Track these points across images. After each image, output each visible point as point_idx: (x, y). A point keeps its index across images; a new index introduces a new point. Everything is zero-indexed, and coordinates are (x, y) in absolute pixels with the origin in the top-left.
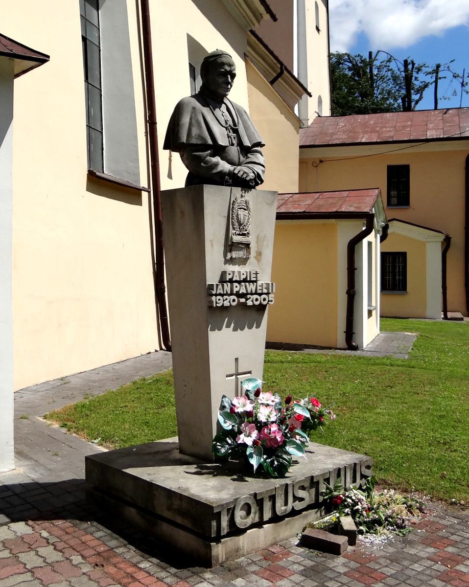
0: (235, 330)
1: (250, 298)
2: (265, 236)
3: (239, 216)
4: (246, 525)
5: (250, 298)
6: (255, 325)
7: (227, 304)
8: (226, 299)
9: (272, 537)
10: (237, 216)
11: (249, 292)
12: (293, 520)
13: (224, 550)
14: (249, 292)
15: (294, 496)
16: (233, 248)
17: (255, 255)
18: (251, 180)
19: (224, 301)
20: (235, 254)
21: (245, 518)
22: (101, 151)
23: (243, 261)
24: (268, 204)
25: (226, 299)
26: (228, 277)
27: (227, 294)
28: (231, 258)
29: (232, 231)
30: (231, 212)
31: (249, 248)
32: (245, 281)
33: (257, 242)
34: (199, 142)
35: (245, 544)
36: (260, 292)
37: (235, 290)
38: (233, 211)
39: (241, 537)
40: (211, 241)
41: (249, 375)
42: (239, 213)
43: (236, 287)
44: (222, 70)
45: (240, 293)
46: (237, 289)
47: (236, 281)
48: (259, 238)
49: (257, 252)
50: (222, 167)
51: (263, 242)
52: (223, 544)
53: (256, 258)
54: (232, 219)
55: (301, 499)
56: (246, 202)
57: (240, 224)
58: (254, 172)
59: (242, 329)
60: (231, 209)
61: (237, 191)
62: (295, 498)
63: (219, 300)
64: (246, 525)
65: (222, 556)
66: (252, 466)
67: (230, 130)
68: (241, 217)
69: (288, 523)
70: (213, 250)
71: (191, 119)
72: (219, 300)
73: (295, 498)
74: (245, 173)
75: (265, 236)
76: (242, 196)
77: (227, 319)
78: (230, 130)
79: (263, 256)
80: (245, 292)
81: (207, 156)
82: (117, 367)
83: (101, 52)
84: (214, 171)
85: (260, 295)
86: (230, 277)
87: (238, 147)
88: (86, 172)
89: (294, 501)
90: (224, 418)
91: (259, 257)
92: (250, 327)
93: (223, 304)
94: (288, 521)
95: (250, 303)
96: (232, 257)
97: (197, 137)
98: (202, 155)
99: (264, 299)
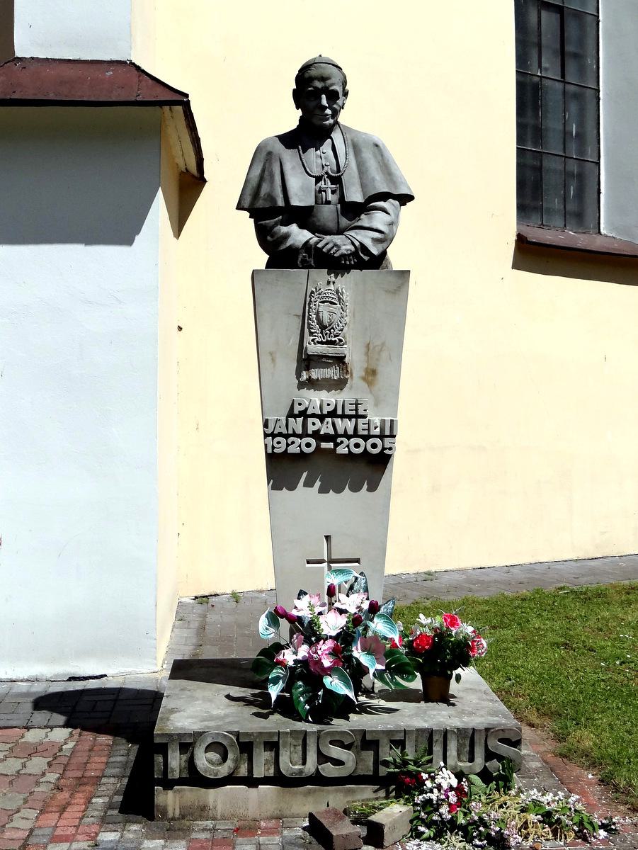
0: (323, 490)
1: (342, 442)
2: (383, 344)
3: (321, 315)
4: (216, 774)
5: (342, 442)
6: (365, 486)
7: (293, 449)
8: (293, 443)
9: (274, 806)
10: (317, 314)
11: (341, 431)
12: (323, 791)
13: (178, 802)
14: (341, 431)
15: (319, 753)
16: (312, 363)
18: (343, 256)
19: (288, 445)
20: (315, 373)
21: (220, 764)
22: (596, 196)
23: (339, 384)
24: (387, 291)
25: (293, 443)
26: (297, 409)
27: (294, 435)
28: (309, 379)
29: (308, 338)
30: (307, 308)
31: (344, 363)
32: (333, 414)
33: (367, 354)
34: (267, 205)
35: (219, 802)
36: (366, 433)
37: (311, 429)
38: (310, 307)
39: (212, 791)
40: (271, 354)
41: (357, 564)
42: (320, 310)
43: (314, 424)
44: (310, 89)
45: (322, 433)
46: (315, 428)
47: (313, 415)
49: (367, 369)
50: (293, 239)
52: (175, 792)
53: (364, 379)
54: (309, 319)
55: (338, 762)
56: (337, 292)
57: (323, 327)
58: (353, 244)
59: (339, 490)
60: (307, 304)
61: (320, 277)
62: (323, 758)
63: (279, 443)
64: (216, 774)
67: (327, 179)
68: (326, 319)
69: (309, 792)
70: (274, 366)
71: (263, 170)
72: (279, 443)
73: (323, 758)
74: (335, 245)
75: (383, 344)
76: (329, 283)
77: (305, 474)
78: (327, 179)
79: (379, 377)
80: (332, 432)
81: (276, 224)
82: (538, 567)
83: (600, 23)
84: (283, 247)
85: (366, 438)
86: (302, 408)
87: (339, 206)
88: (514, 238)
89: (320, 762)
90: (269, 622)
91: (370, 378)
92: (356, 488)
93: (286, 449)
95: (342, 450)
96: (310, 377)
97: (266, 196)
98: (268, 223)
99: (374, 446)
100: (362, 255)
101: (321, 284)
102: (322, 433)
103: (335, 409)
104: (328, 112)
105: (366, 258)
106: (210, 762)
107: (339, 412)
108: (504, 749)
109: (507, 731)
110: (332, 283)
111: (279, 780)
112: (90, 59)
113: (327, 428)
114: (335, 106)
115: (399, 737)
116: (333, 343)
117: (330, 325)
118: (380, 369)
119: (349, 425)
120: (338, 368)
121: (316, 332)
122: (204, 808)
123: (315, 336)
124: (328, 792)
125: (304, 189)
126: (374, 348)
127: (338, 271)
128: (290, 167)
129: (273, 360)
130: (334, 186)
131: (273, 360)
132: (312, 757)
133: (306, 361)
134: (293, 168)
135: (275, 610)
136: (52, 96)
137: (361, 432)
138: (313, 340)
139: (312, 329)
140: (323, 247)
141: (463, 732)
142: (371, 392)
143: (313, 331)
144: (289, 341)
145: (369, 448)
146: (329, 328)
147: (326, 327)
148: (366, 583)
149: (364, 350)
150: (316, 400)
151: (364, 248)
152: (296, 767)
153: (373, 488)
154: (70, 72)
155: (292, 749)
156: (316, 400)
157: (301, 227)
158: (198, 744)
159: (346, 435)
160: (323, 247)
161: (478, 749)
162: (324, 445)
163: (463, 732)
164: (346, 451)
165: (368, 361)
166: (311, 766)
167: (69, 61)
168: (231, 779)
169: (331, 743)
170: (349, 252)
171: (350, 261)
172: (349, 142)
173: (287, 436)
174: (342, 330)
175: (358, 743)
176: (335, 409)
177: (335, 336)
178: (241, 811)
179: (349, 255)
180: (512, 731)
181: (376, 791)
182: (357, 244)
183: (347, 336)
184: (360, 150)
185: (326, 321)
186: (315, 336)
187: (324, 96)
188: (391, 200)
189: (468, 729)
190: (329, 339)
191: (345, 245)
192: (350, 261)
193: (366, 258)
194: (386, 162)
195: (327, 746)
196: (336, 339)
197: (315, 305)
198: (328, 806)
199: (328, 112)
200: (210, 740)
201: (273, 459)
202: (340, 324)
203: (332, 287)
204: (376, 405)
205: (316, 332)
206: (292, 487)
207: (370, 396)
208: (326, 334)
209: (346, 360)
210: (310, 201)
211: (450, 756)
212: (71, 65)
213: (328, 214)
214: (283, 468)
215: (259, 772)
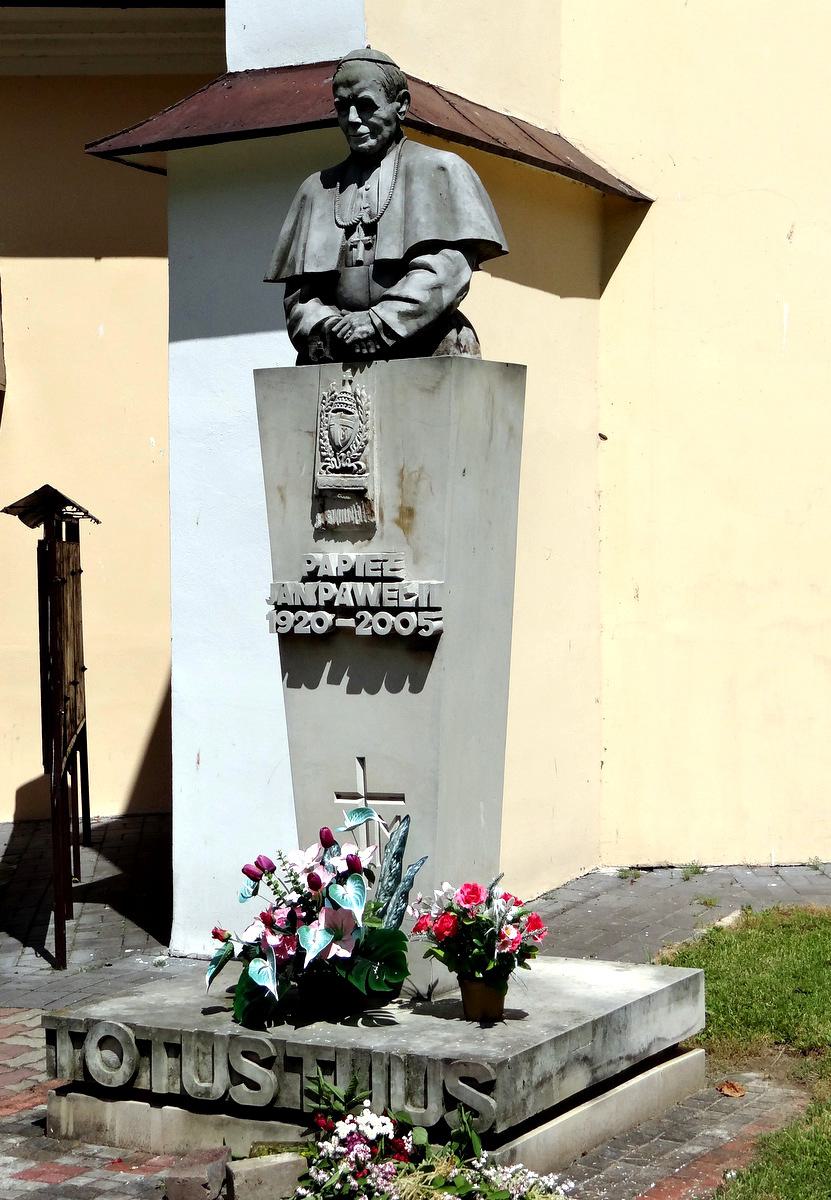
0: (352, 690)
2: (422, 469)
5: (362, 618)
6: (407, 685)
12: (238, 1124)
17: (396, 515)
18: (357, 341)
20: (335, 516)
24: (424, 390)
28: (325, 525)
31: (366, 500)
32: (350, 576)
33: (400, 485)
36: (394, 604)
37: (324, 597)
39: (109, 1105)
45: (336, 604)
46: (329, 597)
48: (406, 474)
49: (401, 508)
51: (416, 483)
53: (398, 523)
55: (253, 1085)
57: (336, 449)
59: (373, 690)
62: (236, 1078)
64: (110, 1082)
65: (68, 1124)
66: (264, 989)
70: (285, 507)
73: (236, 1078)
75: (422, 469)
77: (328, 665)
79: (419, 519)
91: (407, 521)
92: (395, 688)
93: (292, 629)
94: (223, 1120)
95: (363, 630)
96: (326, 522)
100: (385, 338)
101: (335, 384)
102: (336, 604)
103: (353, 570)
104: (364, 129)
105: (390, 342)
106: (106, 1063)
107: (359, 573)
108: (468, 1094)
109: (471, 1067)
110: (347, 383)
111: (182, 1100)
112: (315, 61)
113: (344, 595)
114: (372, 120)
115: (328, 1057)
116: (349, 470)
117: (345, 444)
118: (418, 508)
119: (367, 592)
120: (359, 507)
121: (328, 456)
122: (100, 1128)
123: (327, 461)
124: (245, 1127)
125: (326, 247)
126: (410, 475)
127: (356, 364)
128: (319, 215)
129: (283, 498)
130: (368, 238)
131: (283, 498)
132: (222, 1076)
133: (323, 499)
134: (322, 217)
135: (256, 863)
136: (226, 129)
137: (387, 603)
138: (324, 468)
139: (324, 451)
140: (339, 330)
141: (415, 1061)
142: (408, 543)
143: (324, 454)
144: (301, 468)
145: (400, 628)
146: (344, 449)
147: (339, 448)
148: (407, 830)
149: (397, 479)
150: (335, 556)
151: (386, 328)
152: (203, 1085)
153: (416, 688)
154: (278, 84)
155: (201, 1058)
156: (335, 556)
157: (326, 302)
158: (89, 1036)
159: (367, 608)
160: (339, 330)
161: (432, 1088)
162: (341, 622)
163: (415, 1061)
164: (368, 631)
165: (402, 497)
166: (218, 1085)
167: (291, 68)
168: (127, 1091)
169: (246, 1054)
170: (365, 336)
171: (368, 348)
172: (402, 168)
173: (294, 609)
174: (361, 451)
175: (280, 1060)
176: (353, 570)
177: (353, 461)
178: (143, 1138)
179: (365, 340)
180: (479, 1068)
181: (303, 1135)
182: (377, 322)
183: (369, 460)
184: (411, 180)
185: (339, 441)
186: (327, 461)
187: (353, 108)
188: (447, 251)
189: (422, 1056)
190: (344, 465)
191: (361, 325)
192: (368, 348)
193: (390, 342)
194: (452, 191)
195: (238, 1058)
196: (353, 464)
197: (327, 416)
198: (224, 1144)
199: (364, 129)
200: (101, 1033)
201: (289, 642)
202: (358, 443)
203: (348, 388)
204: (416, 561)
205: (328, 456)
206: (313, 684)
207: (407, 548)
208: (341, 458)
209: (369, 495)
210: (330, 264)
211: (395, 1094)
212: (289, 75)
213: (355, 281)
214: (304, 655)
215: (161, 1086)
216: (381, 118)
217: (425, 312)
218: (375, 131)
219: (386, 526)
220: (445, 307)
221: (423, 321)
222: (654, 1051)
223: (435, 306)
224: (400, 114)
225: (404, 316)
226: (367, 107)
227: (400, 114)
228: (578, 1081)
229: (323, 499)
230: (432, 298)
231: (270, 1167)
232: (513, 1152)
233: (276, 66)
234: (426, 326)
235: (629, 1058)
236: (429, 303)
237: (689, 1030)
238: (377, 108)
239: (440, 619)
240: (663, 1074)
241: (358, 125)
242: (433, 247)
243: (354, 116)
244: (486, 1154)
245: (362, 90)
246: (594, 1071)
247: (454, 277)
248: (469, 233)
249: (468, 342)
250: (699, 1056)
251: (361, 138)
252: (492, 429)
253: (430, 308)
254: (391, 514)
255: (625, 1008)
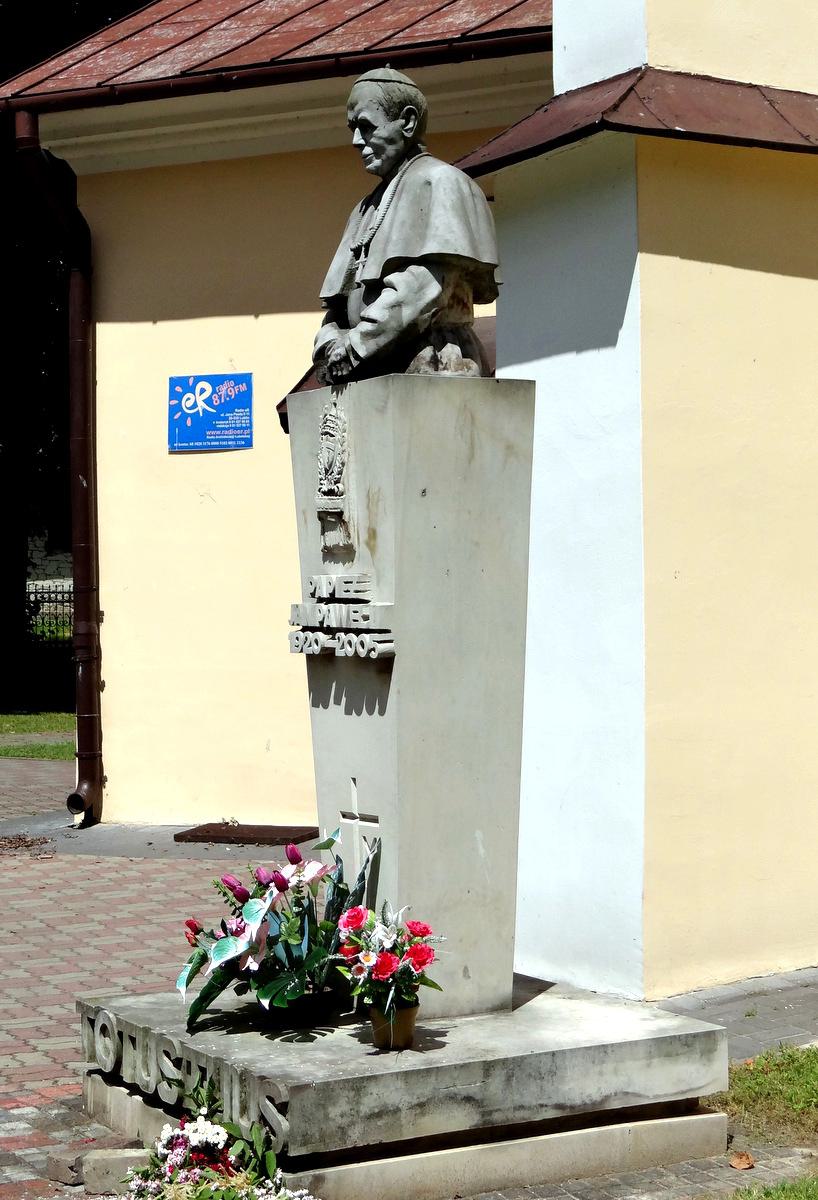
0: (348, 712)
77: (334, 684)
112: (612, 76)
114: (373, 140)
129: (306, 521)
133: (323, 516)
156: (334, 576)
164: (350, 651)
188: (413, 268)
199: (368, 150)
209: (346, 517)
216: (380, 138)
217: (383, 332)
218: (378, 151)
219: (361, 550)
220: (405, 325)
221: (382, 340)
222: (616, 1105)
223: (394, 324)
224: (406, 131)
225: (366, 335)
226: (367, 127)
227: (406, 131)
228: (460, 1120)
229: (323, 516)
230: (391, 317)
231: (116, 1159)
232: (319, 1180)
233: (585, 85)
234: (386, 346)
235: (559, 1107)
236: (387, 322)
237: (691, 1090)
238: (375, 128)
239: (391, 641)
240: (648, 1129)
241: (361, 147)
242: (397, 264)
243: (358, 139)
244: (280, 1173)
245: (359, 113)
246: (483, 1114)
247: (416, 293)
248: (431, 248)
249: (449, 360)
250: (719, 1122)
251: (366, 160)
252: (472, 447)
253: (389, 326)
254: (364, 536)
255: (553, 1054)
